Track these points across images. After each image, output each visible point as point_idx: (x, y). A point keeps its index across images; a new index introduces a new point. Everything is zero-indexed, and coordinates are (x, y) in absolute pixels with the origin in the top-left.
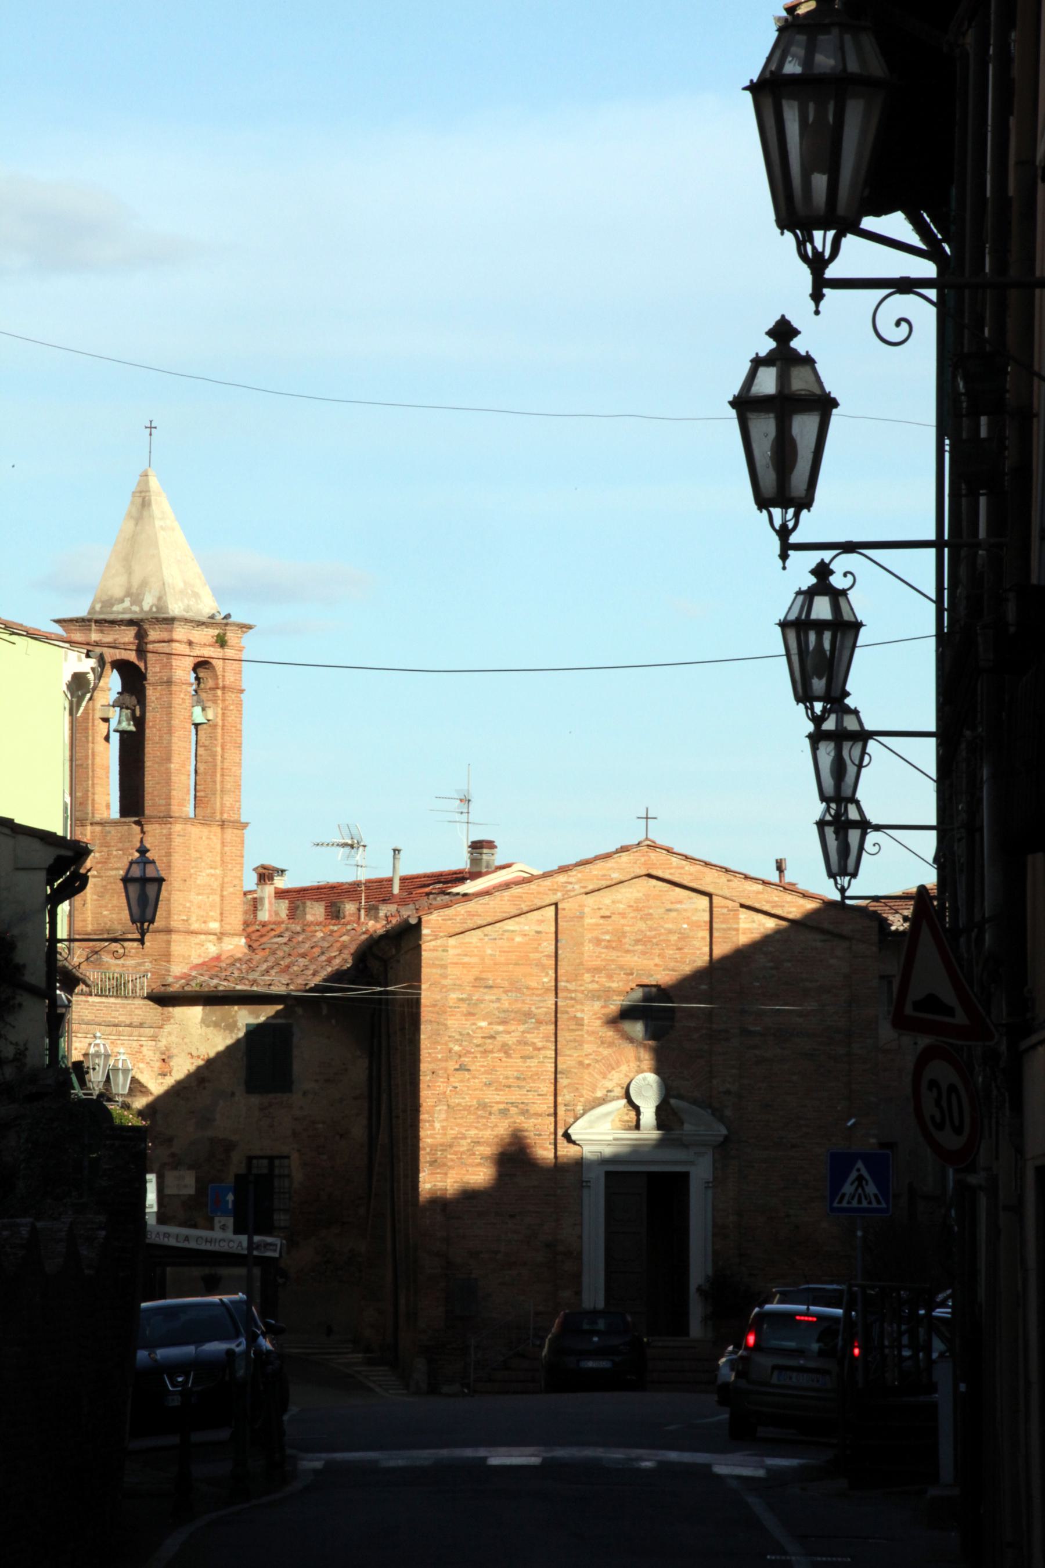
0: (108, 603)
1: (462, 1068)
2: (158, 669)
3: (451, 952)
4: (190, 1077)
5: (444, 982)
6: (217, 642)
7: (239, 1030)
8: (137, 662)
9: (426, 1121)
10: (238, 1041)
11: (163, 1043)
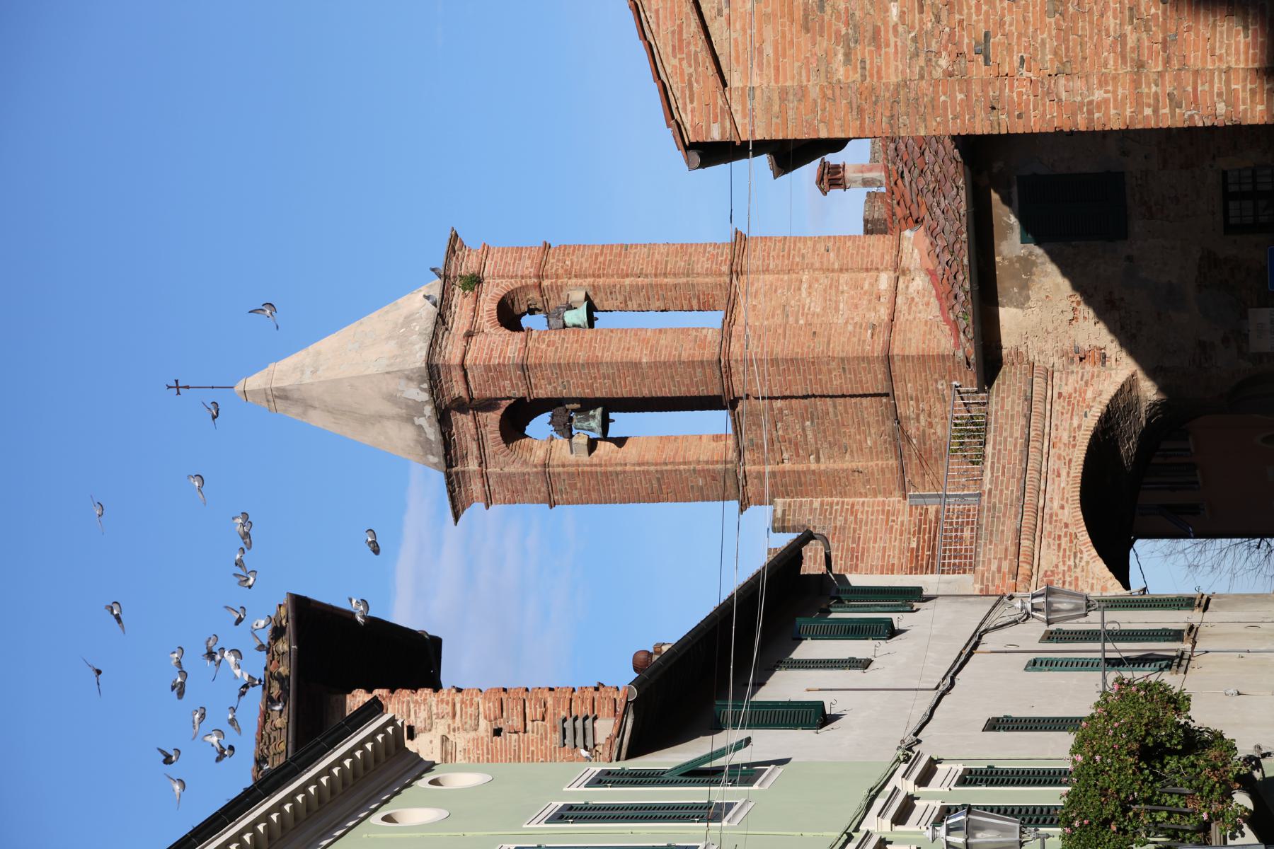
0: (426, 445)
1: (984, 49)
3: (756, 82)
4: (1101, 315)
5: (814, 92)
6: (472, 290)
7: (1031, 254)
8: (502, 410)
9: (1091, 120)
11: (1056, 361)
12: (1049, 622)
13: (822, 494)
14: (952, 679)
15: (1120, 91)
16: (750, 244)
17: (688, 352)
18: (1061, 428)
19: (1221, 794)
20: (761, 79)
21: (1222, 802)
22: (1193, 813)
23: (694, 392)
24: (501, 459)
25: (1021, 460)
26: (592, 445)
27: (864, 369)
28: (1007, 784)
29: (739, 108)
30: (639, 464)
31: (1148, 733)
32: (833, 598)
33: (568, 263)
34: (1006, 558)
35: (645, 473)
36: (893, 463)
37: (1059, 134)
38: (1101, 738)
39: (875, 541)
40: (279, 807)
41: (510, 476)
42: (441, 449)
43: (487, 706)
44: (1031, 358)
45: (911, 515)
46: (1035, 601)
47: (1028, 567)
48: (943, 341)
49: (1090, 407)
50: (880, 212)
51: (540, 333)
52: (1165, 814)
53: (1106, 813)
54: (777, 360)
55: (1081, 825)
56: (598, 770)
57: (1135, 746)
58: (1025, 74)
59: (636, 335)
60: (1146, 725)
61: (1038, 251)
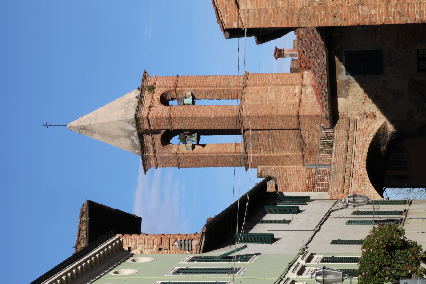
0: (135, 146)
2: (163, 124)
3: (249, 7)
5: (271, 11)
6: (151, 91)
7: (349, 79)
8: (162, 134)
9: (370, 21)
10: (356, 79)
12: (354, 206)
13: (275, 164)
14: (320, 227)
15: (381, 10)
16: (250, 76)
17: (227, 113)
18: (359, 141)
19: (416, 264)
20: (252, 6)
21: (416, 267)
22: (406, 270)
23: (230, 128)
24: (161, 151)
25: (345, 152)
26: (193, 147)
27: (290, 120)
28: (339, 262)
29: (244, 16)
30: (210, 153)
31: (389, 242)
32: (278, 200)
33: (185, 82)
34: (339, 186)
35: (212, 156)
36: (300, 153)
37: (359, 26)
38: (372, 243)
39: (293, 181)
40: (76, 267)
41: (164, 157)
42: (140, 148)
43: (156, 240)
44: (349, 116)
45: (306, 172)
46: (349, 199)
47: (347, 189)
48: (318, 110)
49: (370, 134)
50: (296, 66)
51: (175, 107)
52: (395, 271)
53: (374, 270)
54: (259, 116)
55: (365, 274)
56: (192, 256)
57: (385, 246)
58: (347, 4)
59: (209, 107)
60: (389, 239)
61: (352, 78)
